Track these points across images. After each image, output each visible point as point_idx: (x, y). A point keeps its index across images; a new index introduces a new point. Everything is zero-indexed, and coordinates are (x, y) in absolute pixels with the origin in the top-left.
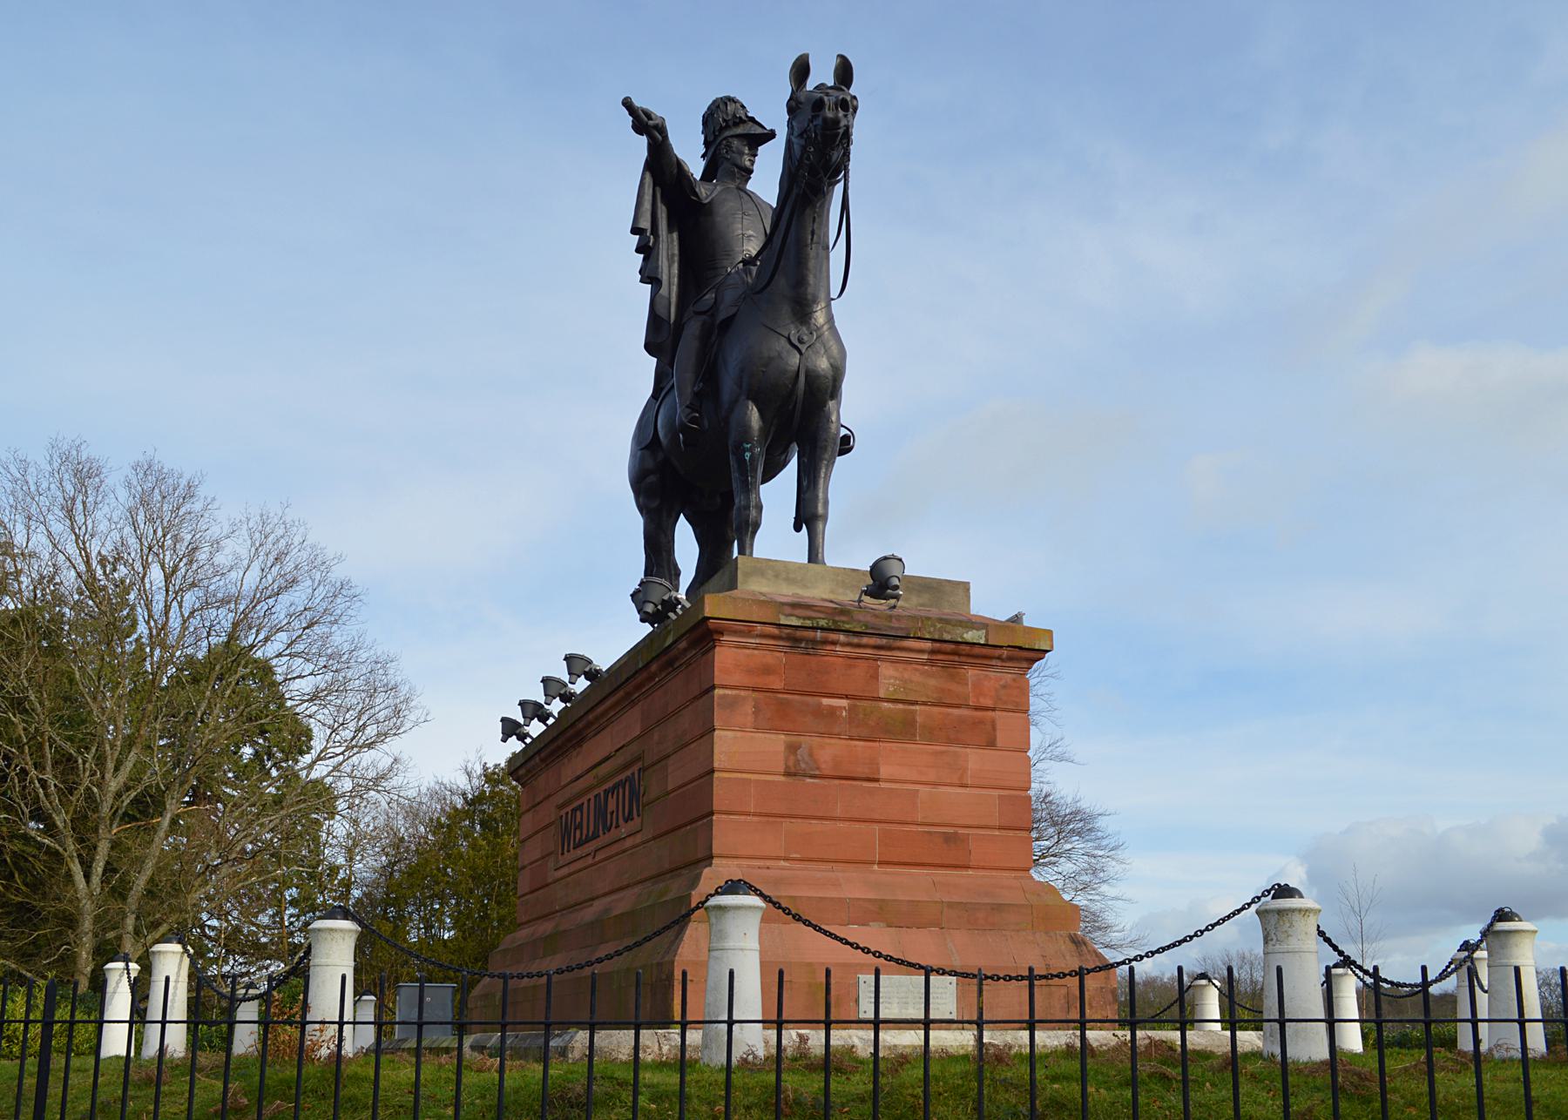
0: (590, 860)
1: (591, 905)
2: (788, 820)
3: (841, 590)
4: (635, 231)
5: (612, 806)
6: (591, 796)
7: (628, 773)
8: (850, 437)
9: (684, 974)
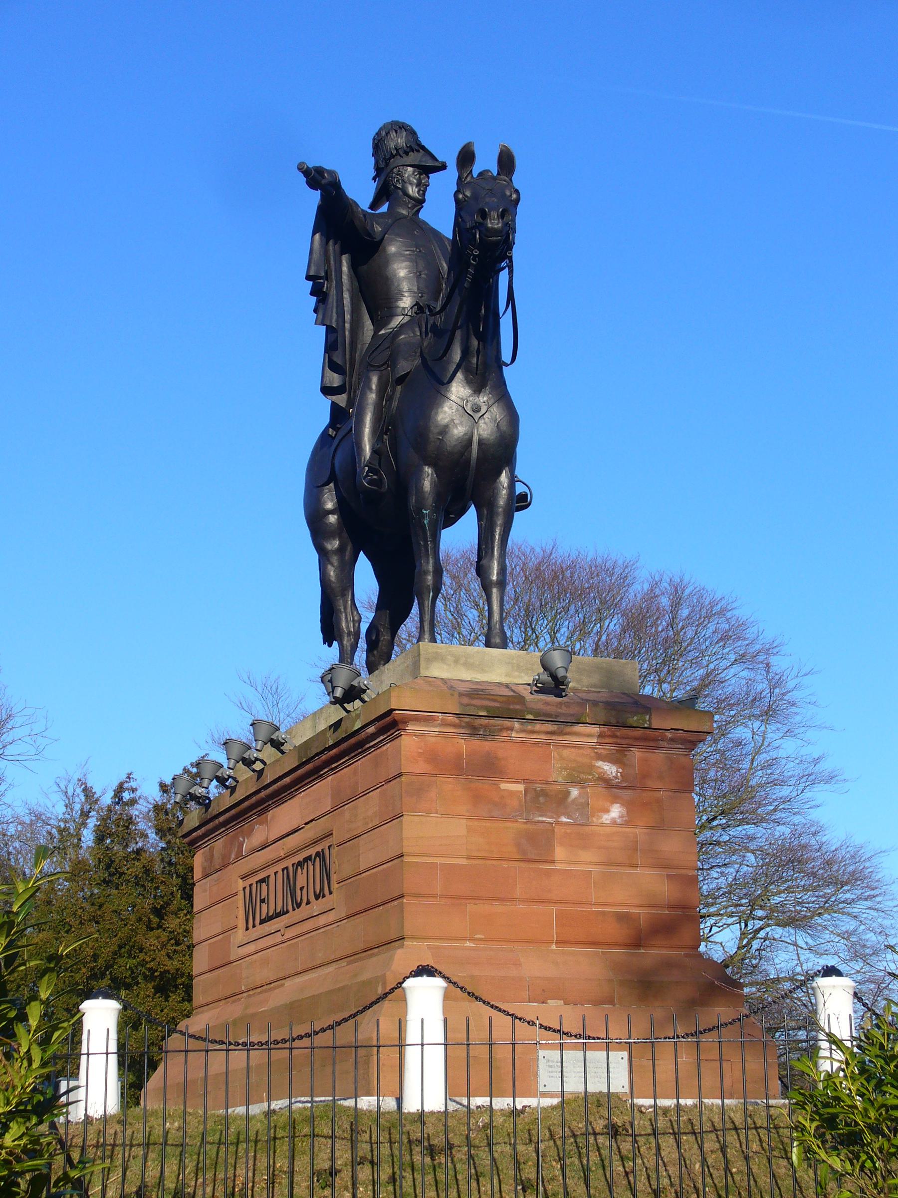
0: (278, 938)
1: (283, 985)
2: (472, 901)
3: (517, 673)
4: (308, 278)
5: (301, 880)
6: (279, 867)
7: (318, 848)
8: (526, 495)
9: (89, 1031)
